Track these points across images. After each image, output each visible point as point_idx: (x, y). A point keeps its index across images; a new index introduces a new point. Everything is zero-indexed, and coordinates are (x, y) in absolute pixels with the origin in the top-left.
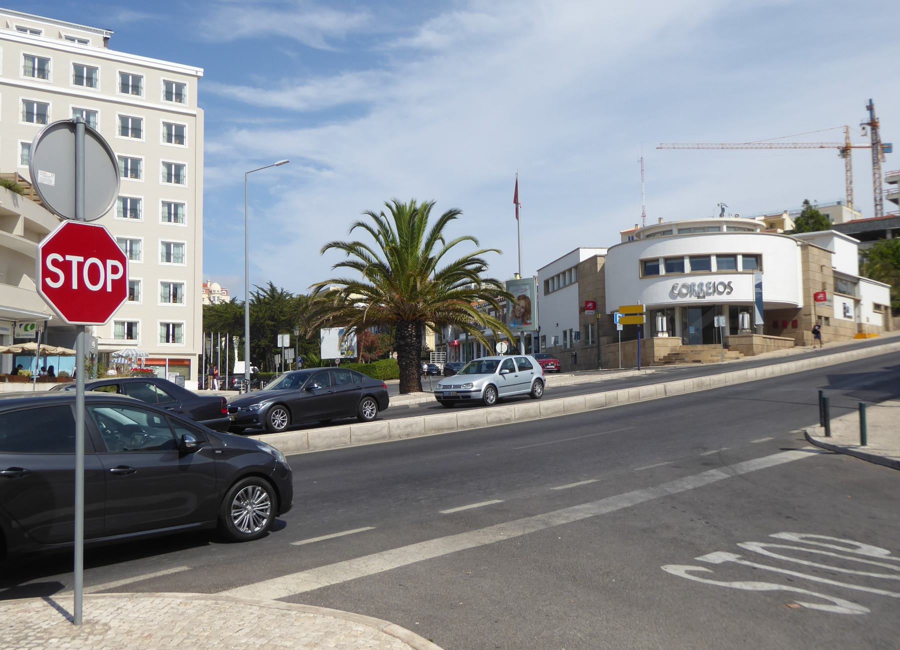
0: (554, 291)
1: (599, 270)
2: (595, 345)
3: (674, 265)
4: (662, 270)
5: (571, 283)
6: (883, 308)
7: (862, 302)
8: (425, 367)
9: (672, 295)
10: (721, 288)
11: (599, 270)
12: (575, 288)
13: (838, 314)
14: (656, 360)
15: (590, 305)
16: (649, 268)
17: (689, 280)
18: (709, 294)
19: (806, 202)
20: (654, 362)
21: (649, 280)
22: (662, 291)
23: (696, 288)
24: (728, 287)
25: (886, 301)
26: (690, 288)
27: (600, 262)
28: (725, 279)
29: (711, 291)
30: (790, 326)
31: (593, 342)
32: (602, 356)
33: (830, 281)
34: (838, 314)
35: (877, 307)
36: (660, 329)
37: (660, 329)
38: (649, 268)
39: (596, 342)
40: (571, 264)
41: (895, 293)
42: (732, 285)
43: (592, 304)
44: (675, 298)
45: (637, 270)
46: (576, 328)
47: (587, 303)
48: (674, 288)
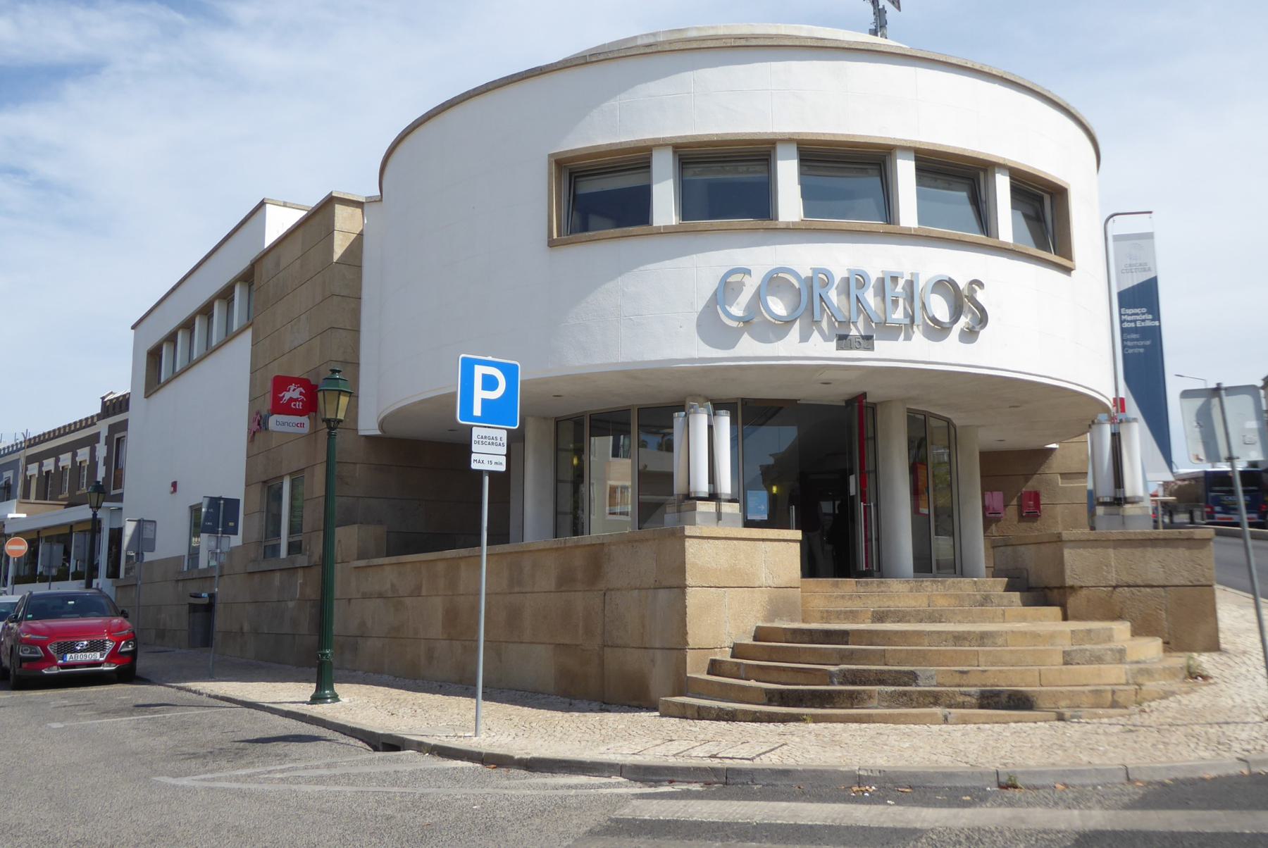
0: (175, 376)
1: (338, 251)
2: (301, 560)
3: (728, 182)
4: (665, 203)
5: (229, 337)
8: (775, 489)
9: (711, 323)
10: (940, 308)
11: (338, 251)
12: (242, 347)
14: (696, 670)
15: (294, 393)
16: (600, 197)
17: (803, 258)
18: (891, 331)
20: (684, 685)
21: (600, 252)
22: (665, 308)
23: (833, 296)
24: (965, 305)
26: (808, 299)
27: (346, 223)
29: (898, 315)
31: (294, 548)
32: (338, 611)
36: (703, 487)
37: (703, 487)
38: (600, 197)
39: (316, 548)
40: (234, 262)
42: (980, 296)
43: (302, 393)
44: (726, 337)
45: (535, 200)
46: (233, 486)
47: (281, 383)
48: (726, 289)
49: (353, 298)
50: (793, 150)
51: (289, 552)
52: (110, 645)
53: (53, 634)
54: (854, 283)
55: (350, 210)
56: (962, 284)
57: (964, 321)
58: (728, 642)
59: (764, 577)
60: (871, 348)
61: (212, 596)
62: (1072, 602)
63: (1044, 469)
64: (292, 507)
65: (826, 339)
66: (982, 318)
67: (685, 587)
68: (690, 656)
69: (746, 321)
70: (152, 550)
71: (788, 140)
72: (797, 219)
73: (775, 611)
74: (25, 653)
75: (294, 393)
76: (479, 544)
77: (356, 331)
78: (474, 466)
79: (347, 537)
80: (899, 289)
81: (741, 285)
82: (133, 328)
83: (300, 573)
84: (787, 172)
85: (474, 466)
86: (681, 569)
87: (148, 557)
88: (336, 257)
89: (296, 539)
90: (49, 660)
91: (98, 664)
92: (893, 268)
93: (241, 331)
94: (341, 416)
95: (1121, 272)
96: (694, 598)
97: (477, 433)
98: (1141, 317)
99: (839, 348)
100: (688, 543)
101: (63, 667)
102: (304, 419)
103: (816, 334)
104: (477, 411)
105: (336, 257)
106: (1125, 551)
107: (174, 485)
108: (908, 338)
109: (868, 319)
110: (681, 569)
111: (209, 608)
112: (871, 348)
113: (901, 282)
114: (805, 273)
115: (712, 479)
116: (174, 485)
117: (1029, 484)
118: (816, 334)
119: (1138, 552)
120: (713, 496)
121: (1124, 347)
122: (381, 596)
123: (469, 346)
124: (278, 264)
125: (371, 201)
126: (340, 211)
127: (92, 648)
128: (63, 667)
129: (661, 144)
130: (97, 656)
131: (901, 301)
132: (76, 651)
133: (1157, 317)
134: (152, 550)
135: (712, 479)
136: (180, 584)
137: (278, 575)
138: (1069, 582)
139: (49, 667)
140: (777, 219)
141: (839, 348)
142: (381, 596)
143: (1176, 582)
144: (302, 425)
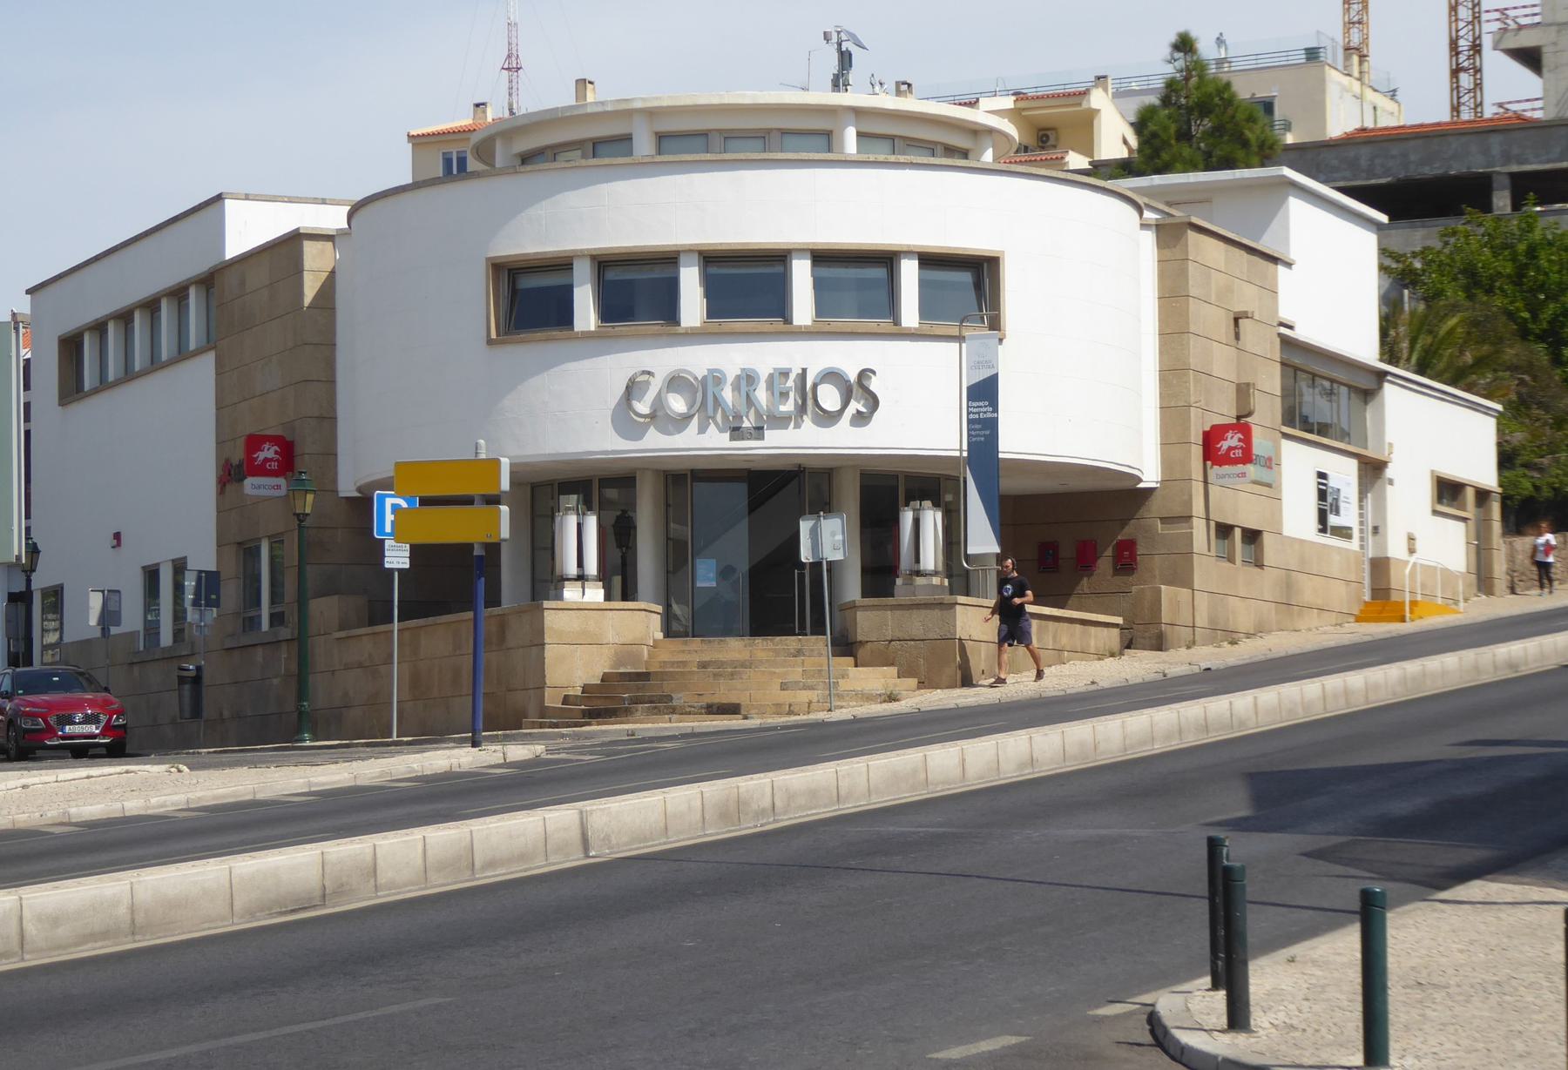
1: (309, 294)
2: (285, 633)
3: (637, 290)
4: (586, 312)
5: (183, 354)
6: (1470, 494)
7: (1390, 472)
10: (829, 398)
11: (309, 294)
12: (201, 374)
13: (1297, 517)
14: (552, 700)
15: (268, 452)
16: (530, 300)
17: (698, 359)
18: (781, 421)
19: (1184, 44)
20: (544, 712)
22: (584, 403)
23: (728, 395)
24: (860, 392)
25: (1482, 470)
26: (703, 395)
27: (316, 262)
28: (849, 356)
29: (788, 407)
30: (1105, 563)
31: (277, 619)
33: (1270, 381)
34: (1297, 517)
35: (1448, 491)
36: (572, 569)
37: (572, 569)
38: (530, 300)
41: (1519, 437)
43: (274, 449)
45: (475, 304)
46: (204, 557)
47: (254, 442)
48: (632, 389)
49: (327, 345)
50: (696, 256)
51: (272, 624)
52: (103, 718)
53: (51, 706)
54: (748, 379)
55: (319, 245)
56: (852, 376)
57: (855, 406)
58: (579, 683)
59: (611, 637)
60: (761, 437)
61: (199, 669)
62: (861, 653)
63: (1142, 512)
64: (272, 559)
65: (721, 431)
66: (873, 402)
67: (543, 644)
68: (547, 692)
69: (652, 416)
70: (118, 624)
71: (689, 251)
72: (698, 324)
73: (619, 661)
74: (27, 725)
75: (268, 452)
76: (391, 621)
77: (332, 382)
78: (387, 566)
79: (324, 609)
80: (790, 383)
81: (648, 383)
82: (28, 292)
83: (284, 647)
84: (690, 281)
85: (387, 566)
86: (541, 632)
87: (114, 630)
88: (307, 300)
89: (277, 610)
90: (50, 731)
91: (94, 736)
92: (783, 364)
93: (199, 352)
94: (308, 510)
95: (970, 368)
96: (550, 652)
97: (387, 543)
98: (983, 409)
99: (732, 438)
100: (546, 613)
101: (63, 738)
102: (281, 481)
103: (712, 427)
104: (388, 529)
105: (307, 300)
106: (898, 613)
107: (117, 536)
108: (797, 426)
109: (758, 415)
110: (540, 632)
111: (197, 680)
112: (761, 437)
113: (792, 376)
114: (700, 373)
115: (580, 564)
116: (117, 536)
117: (1127, 530)
118: (712, 427)
119: (907, 613)
120: (581, 578)
121: (969, 435)
122: (360, 666)
123: (442, 410)
124: (242, 283)
125: (341, 233)
126: (309, 248)
127: (88, 720)
128: (63, 738)
129: (580, 254)
130: (93, 729)
131: (792, 394)
132: (74, 723)
133: (996, 410)
134: (118, 624)
135: (580, 564)
136: (136, 669)
137: (260, 650)
138: (859, 638)
139: (50, 739)
140: (678, 323)
141: (732, 438)
142: (360, 666)
143: (931, 636)
144: (279, 487)
